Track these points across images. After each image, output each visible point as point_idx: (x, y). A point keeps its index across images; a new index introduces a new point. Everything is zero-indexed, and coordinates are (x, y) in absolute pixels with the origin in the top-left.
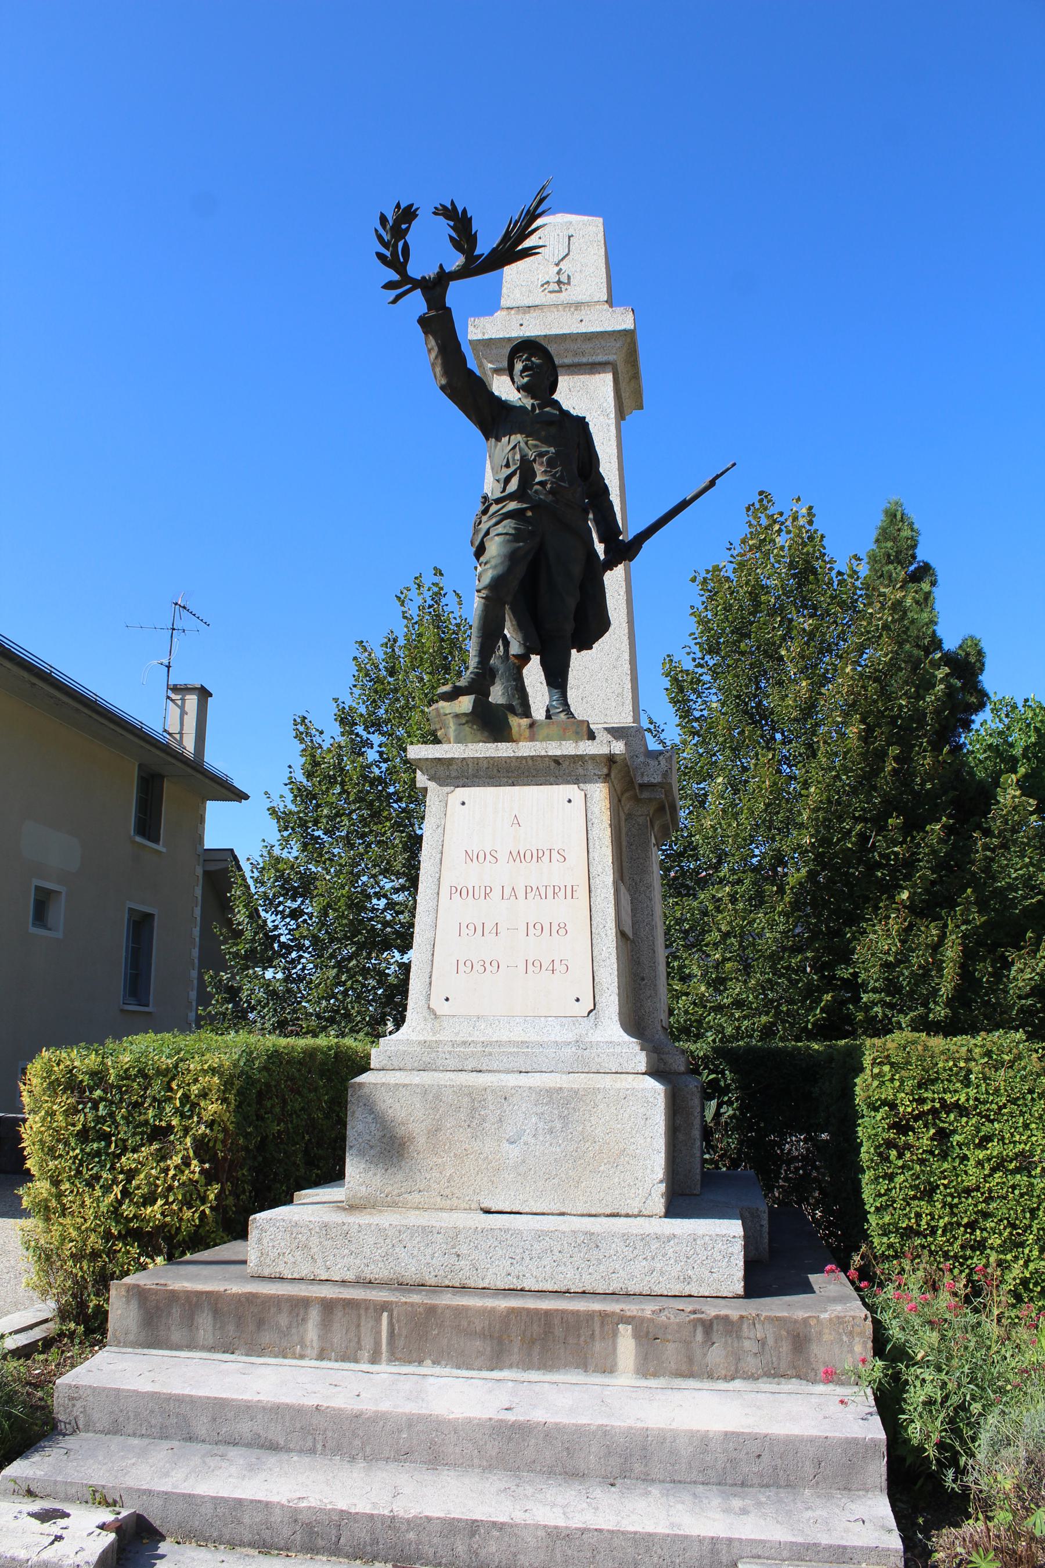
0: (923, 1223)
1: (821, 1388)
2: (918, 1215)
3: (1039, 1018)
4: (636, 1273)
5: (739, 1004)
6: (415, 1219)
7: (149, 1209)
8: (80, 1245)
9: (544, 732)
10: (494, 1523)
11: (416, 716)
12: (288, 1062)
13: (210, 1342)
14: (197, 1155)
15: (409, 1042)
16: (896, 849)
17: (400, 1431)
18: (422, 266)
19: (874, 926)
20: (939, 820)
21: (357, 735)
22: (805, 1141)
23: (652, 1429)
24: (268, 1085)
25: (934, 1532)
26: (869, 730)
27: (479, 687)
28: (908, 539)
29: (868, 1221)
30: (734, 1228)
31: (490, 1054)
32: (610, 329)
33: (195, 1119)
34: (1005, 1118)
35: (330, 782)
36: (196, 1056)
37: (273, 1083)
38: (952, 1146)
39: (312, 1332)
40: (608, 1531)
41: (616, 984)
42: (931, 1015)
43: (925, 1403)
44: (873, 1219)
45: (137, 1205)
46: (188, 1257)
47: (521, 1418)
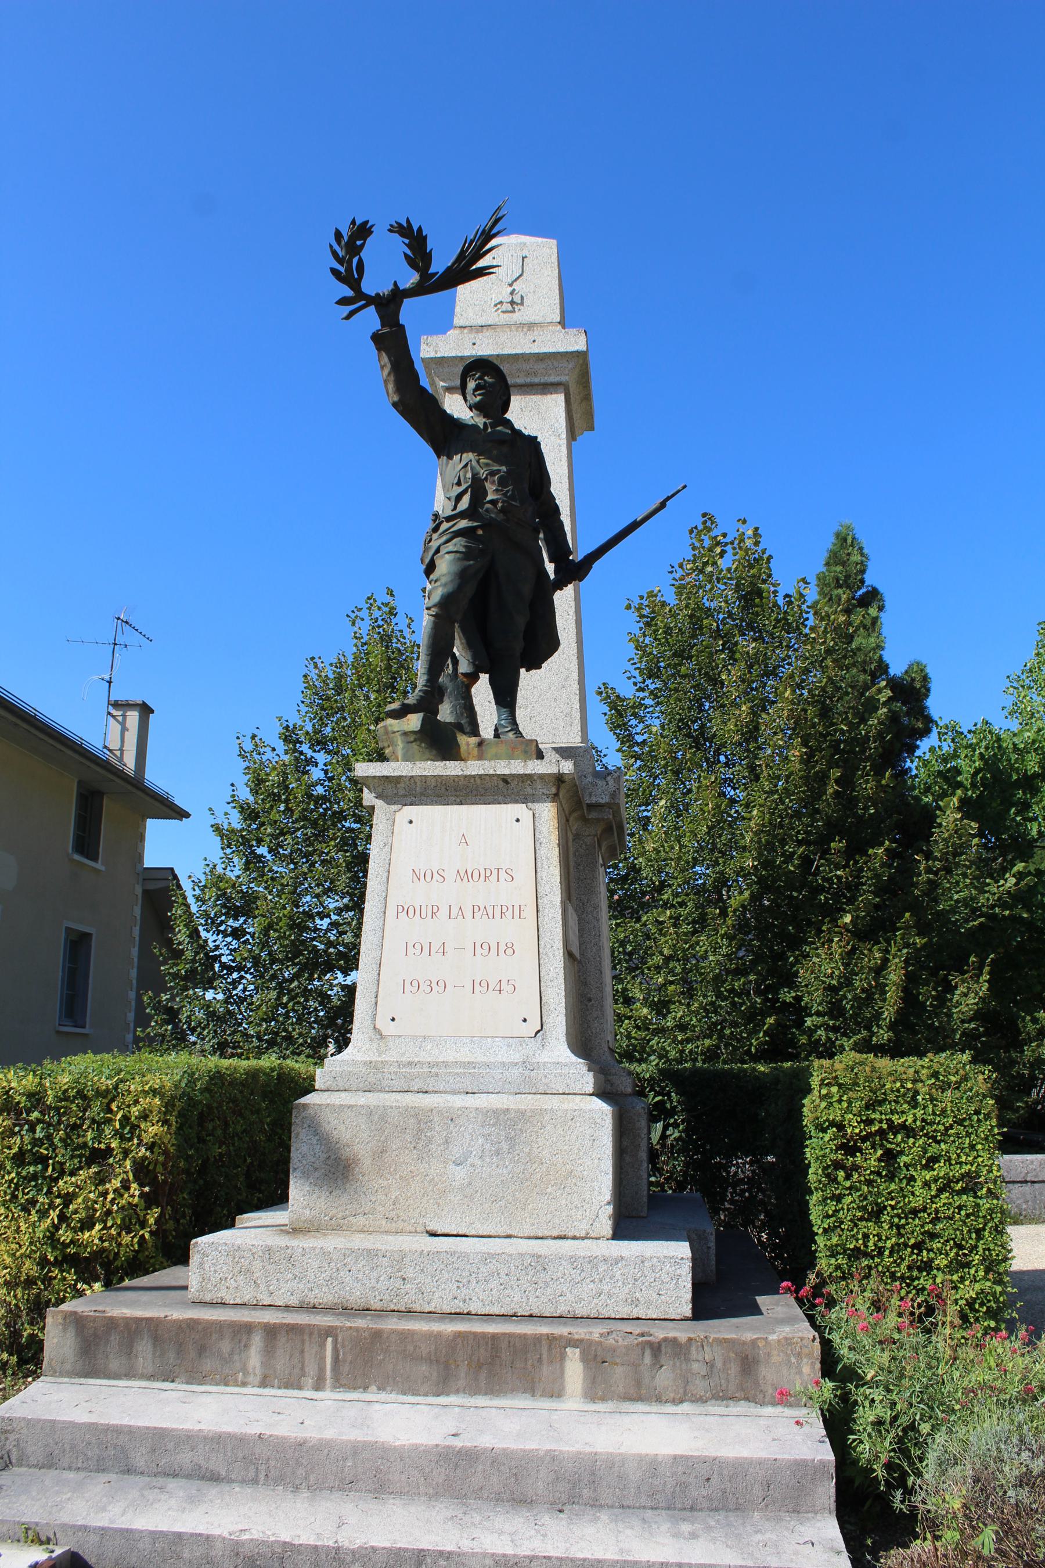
0: (871, 1243)
1: (769, 1410)
2: (866, 1236)
3: (982, 1042)
4: (584, 1296)
5: (682, 1027)
6: (359, 1242)
7: (87, 1234)
8: (15, 1271)
9: (492, 751)
10: (441, 1552)
11: (363, 735)
12: (231, 1083)
13: (150, 1369)
14: (136, 1178)
15: (355, 1063)
16: (839, 873)
17: (345, 1459)
18: (374, 284)
19: (817, 949)
20: (882, 844)
21: (301, 753)
22: (751, 1163)
23: (601, 1453)
24: (209, 1107)
25: (882, 1553)
26: (810, 755)
27: (428, 704)
28: (857, 564)
29: (815, 1243)
30: (682, 1250)
31: (437, 1075)
32: (562, 350)
33: (136, 1141)
34: (952, 1138)
35: (274, 800)
36: (137, 1077)
37: (215, 1105)
38: (899, 1167)
39: (254, 1358)
40: (557, 1558)
41: (563, 1004)
42: (874, 1039)
43: (873, 1424)
44: (820, 1240)
45: (75, 1230)
46: (127, 1282)
47: (469, 1444)
